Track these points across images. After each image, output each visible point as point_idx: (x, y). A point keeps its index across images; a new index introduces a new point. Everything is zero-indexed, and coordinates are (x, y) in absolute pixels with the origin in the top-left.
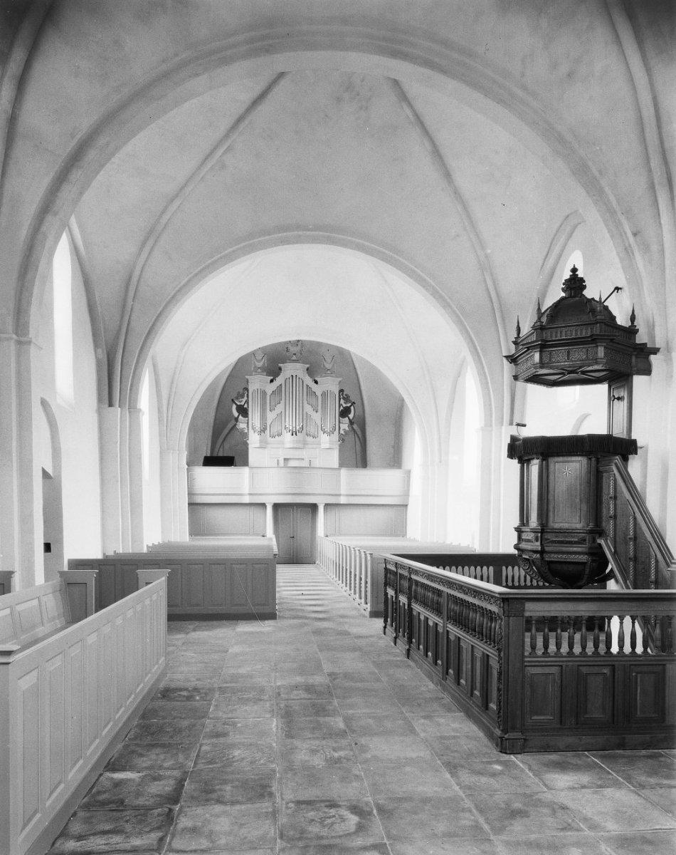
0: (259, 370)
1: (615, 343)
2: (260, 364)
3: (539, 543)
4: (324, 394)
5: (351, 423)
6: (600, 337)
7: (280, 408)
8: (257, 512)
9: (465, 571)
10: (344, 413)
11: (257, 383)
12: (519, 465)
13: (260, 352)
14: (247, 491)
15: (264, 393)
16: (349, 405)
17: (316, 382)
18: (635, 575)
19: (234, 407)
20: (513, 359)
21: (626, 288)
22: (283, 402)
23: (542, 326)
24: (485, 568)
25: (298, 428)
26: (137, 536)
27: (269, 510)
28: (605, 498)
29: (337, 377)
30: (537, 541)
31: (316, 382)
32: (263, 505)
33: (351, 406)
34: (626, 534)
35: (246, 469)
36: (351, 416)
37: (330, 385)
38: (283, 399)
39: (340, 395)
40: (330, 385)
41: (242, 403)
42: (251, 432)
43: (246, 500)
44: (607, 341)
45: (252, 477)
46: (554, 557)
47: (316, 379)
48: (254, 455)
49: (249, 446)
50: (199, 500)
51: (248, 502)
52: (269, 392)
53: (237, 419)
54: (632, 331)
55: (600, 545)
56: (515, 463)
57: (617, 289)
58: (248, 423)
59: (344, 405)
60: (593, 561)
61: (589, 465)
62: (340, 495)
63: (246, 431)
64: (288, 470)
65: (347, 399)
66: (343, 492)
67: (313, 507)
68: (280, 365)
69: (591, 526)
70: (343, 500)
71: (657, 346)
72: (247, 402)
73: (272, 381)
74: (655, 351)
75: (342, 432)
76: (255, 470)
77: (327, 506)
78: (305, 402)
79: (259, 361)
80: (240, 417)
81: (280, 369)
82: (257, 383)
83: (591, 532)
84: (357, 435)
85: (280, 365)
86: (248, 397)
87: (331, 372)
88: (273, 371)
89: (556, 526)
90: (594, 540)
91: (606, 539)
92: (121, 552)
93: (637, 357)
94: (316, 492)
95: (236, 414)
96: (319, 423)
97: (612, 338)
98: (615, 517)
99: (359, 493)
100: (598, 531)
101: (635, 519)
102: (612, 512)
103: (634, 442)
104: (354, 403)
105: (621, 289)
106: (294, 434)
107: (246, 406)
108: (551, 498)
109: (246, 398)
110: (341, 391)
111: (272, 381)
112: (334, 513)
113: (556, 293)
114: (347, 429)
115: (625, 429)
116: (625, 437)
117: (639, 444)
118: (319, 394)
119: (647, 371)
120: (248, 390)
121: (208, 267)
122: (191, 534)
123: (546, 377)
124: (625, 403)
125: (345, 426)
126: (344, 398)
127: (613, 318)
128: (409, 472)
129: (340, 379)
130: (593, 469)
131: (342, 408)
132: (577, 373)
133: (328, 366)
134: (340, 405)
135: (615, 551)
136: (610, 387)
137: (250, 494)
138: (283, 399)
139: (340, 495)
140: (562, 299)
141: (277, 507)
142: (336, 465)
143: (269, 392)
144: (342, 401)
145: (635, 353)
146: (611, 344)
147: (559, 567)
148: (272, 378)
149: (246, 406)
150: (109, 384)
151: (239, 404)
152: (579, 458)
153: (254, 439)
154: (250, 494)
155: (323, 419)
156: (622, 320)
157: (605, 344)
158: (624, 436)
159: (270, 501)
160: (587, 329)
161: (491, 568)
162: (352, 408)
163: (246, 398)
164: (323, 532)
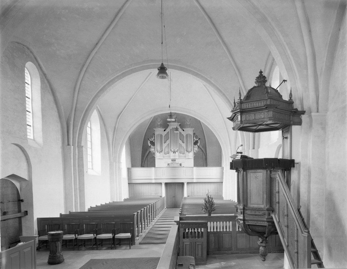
0: (159, 126)
1: (278, 109)
2: (159, 124)
3: (242, 215)
4: (187, 135)
5: (199, 147)
6: (269, 106)
7: (168, 142)
8: (159, 187)
9: (221, 223)
10: (196, 143)
11: (159, 131)
12: (236, 173)
13: (159, 120)
14: (153, 178)
15: (161, 136)
16: (197, 140)
17: (183, 130)
18: (288, 236)
19: (149, 142)
20: (232, 119)
21: (288, 81)
22: (169, 139)
23: (241, 101)
24: (228, 222)
25: (176, 150)
26: (83, 204)
27: (163, 185)
28: (274, 192)
29: (192, 128)
30: (242, 214)
31: (183, 130)
32: (161, 184)
33: (198, 140)
34: (283, 213)
35: (153, 169)
36: (198, 144)
37: (189, 131)
38: (170, 138)
39: (193, 136)
40: (189, 131)
41: (152, 140)
42: (156, 152)
43: (153, 181)
44: (274, 108)
45: (156, 172)
46: (250, 223)
47: (183, 129)
48: (158, 163)
49: (156, 158)
50: (134, 182)
51: (154, 182)
52: (163, 135)
53: (150, 147)
54: (290, 103)
55: (272, 218)
56: (234, 173)
57: (284, 81)
58: (155, 148)
59: (196, 140)
60: (269, 225)
61: (265, 174)
62: (193, 179)
63: (154, 152)
64: (170, 169)
65: (196, 137)
66: (194, 177)
67: (182, 184)
68: (168, 123)
69: (268, 207)
70: (195, 181)
71: (304, 110)
72: (154, 139)
73: (165, 130)
74: (303, 112)
75: (195, 151)
76: (157, 169)
77: (188, 183)
78: (179, 139)
79: (159, 122)
80: (152, 146)
81: (168, 125)
82: (159, 131)
83: (268, 210)
84: (204, 153)
85: (168, 123)
86: (155, 137)
87: (190, 126)
88: (165, 125)
89: (252, 206)
90: (269, 214)
91: (275, 214)
92: (74, 211)
93: (293, 116)
94: (183, 176)
95: (150, 145)
96: (185, 148)
97: (277, 106)
98: (279, 203)
99: (201, 178)
100: (271, 210)
101: (287, 204)
102: (277, 200)
103: (293, 161)
104: (200, 139)
105: (286, 81)
106: (174, 153)
107: (154, 141)
108: (248, 191)
109: (154, 138)
110: (194, 134)
111: (165, 130)
112: (191, 186)
113: (251, 83)
114: (197, 150)
115: (289, 155)
116: (289, 159)
117: (296, 162)
118: (185, 135)
119: (300, 123)
120: (155, 135)
121: (111, 81)
122: (38, 219)
123: (248, 128)
124: (289, 139)
125: (196, 149)
126: (195, 137)
127: (281, 96)
128: (223, 168)
129: (194, 129)
130: (268, 176)
131: (194, 141)
132: (263, 125)
133: (188, 124)
134: (194, 140)
135: (279, 221)
136: (283, 132)
137: (155, 179)
138: (170, 138)
139: (193, 179)
140: (255, 87)
141: (166, 184)
142: (193, 166)
143: (163, 135)
144: (195, 138)
145: (292, 114)
146: (276, 109)
147: (254, 228)
148: (164, 129)
149: (154, 141)
150: (67, 135)
151: (151, 140)
152: (262, 171)
153: (158, 155)
154: (155, 179)
155: (187, 146)
156: (286, 97)
157: (273, 110)
158: (289, 159)
159: (164, 181)
160: (261, 103)
161: (231, 222)
162: (199, 141)
163: (154, 138)
164: (186, 195)
